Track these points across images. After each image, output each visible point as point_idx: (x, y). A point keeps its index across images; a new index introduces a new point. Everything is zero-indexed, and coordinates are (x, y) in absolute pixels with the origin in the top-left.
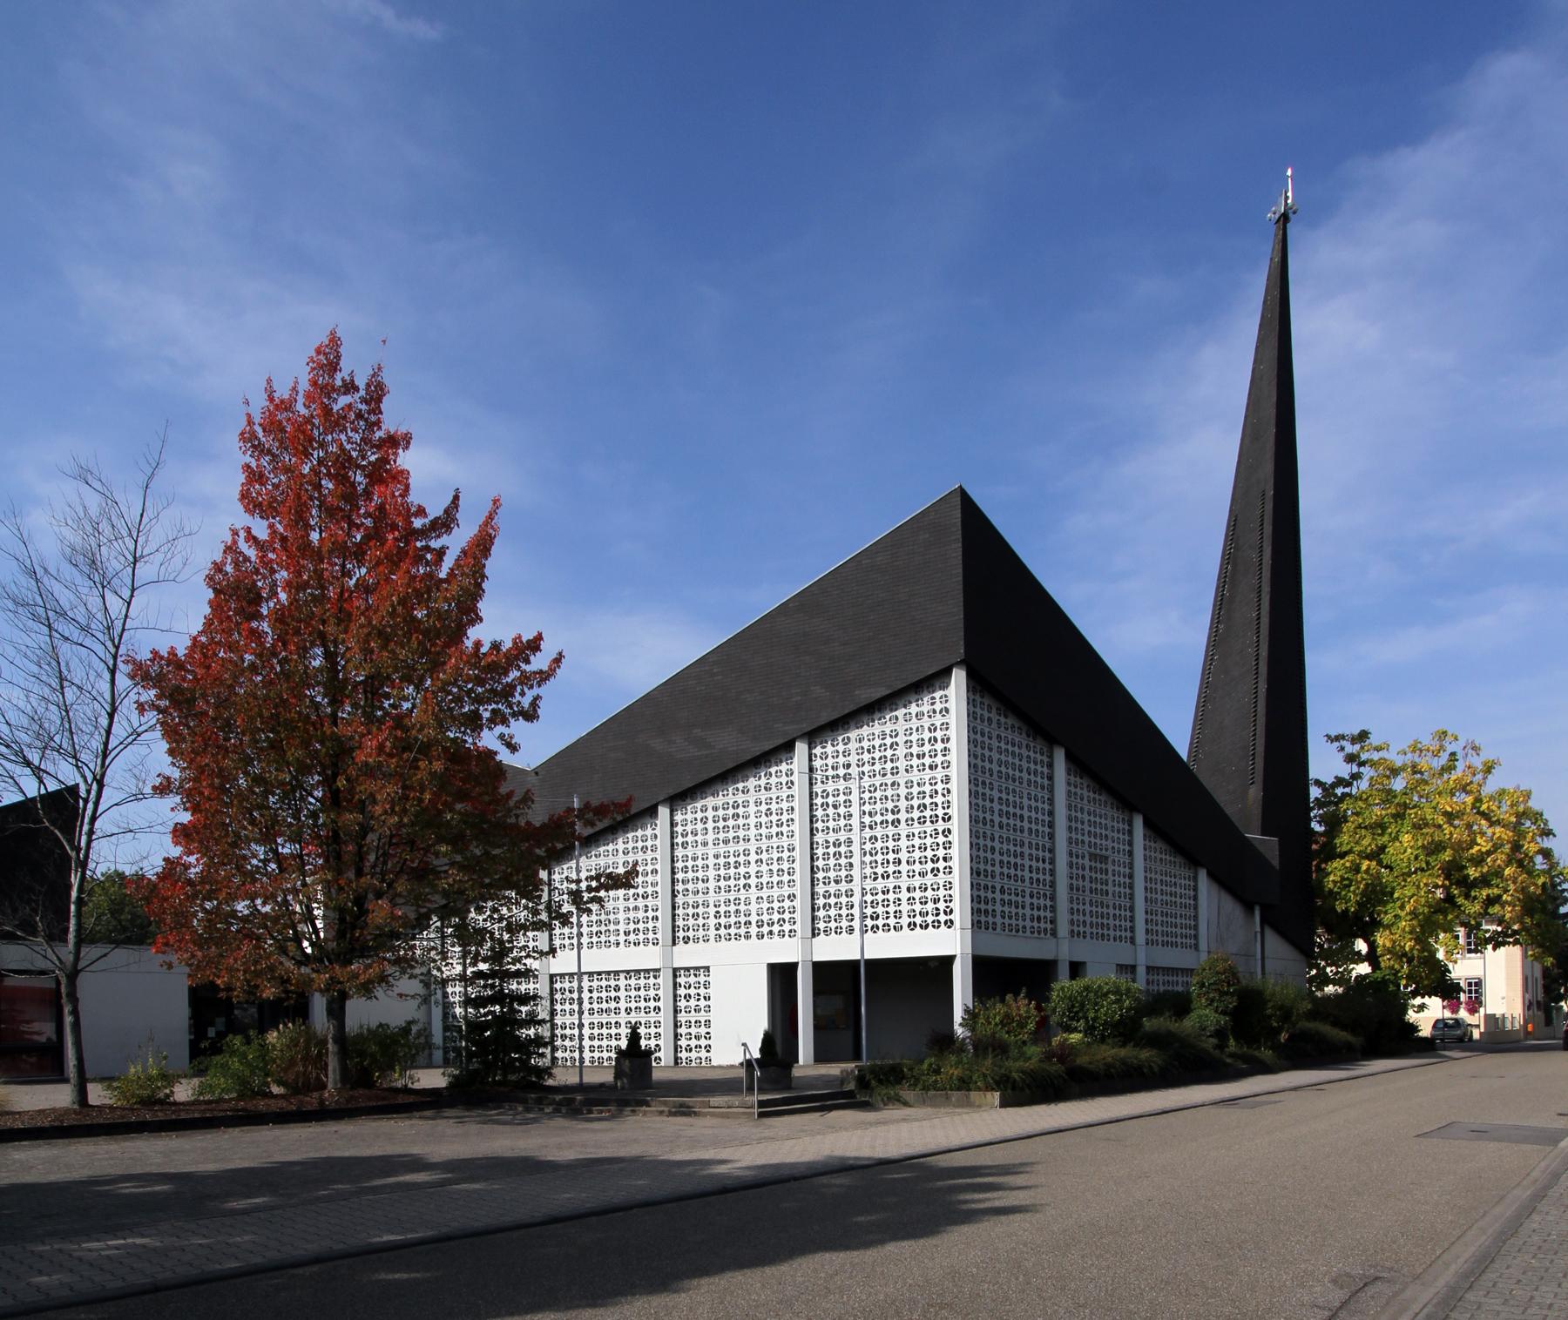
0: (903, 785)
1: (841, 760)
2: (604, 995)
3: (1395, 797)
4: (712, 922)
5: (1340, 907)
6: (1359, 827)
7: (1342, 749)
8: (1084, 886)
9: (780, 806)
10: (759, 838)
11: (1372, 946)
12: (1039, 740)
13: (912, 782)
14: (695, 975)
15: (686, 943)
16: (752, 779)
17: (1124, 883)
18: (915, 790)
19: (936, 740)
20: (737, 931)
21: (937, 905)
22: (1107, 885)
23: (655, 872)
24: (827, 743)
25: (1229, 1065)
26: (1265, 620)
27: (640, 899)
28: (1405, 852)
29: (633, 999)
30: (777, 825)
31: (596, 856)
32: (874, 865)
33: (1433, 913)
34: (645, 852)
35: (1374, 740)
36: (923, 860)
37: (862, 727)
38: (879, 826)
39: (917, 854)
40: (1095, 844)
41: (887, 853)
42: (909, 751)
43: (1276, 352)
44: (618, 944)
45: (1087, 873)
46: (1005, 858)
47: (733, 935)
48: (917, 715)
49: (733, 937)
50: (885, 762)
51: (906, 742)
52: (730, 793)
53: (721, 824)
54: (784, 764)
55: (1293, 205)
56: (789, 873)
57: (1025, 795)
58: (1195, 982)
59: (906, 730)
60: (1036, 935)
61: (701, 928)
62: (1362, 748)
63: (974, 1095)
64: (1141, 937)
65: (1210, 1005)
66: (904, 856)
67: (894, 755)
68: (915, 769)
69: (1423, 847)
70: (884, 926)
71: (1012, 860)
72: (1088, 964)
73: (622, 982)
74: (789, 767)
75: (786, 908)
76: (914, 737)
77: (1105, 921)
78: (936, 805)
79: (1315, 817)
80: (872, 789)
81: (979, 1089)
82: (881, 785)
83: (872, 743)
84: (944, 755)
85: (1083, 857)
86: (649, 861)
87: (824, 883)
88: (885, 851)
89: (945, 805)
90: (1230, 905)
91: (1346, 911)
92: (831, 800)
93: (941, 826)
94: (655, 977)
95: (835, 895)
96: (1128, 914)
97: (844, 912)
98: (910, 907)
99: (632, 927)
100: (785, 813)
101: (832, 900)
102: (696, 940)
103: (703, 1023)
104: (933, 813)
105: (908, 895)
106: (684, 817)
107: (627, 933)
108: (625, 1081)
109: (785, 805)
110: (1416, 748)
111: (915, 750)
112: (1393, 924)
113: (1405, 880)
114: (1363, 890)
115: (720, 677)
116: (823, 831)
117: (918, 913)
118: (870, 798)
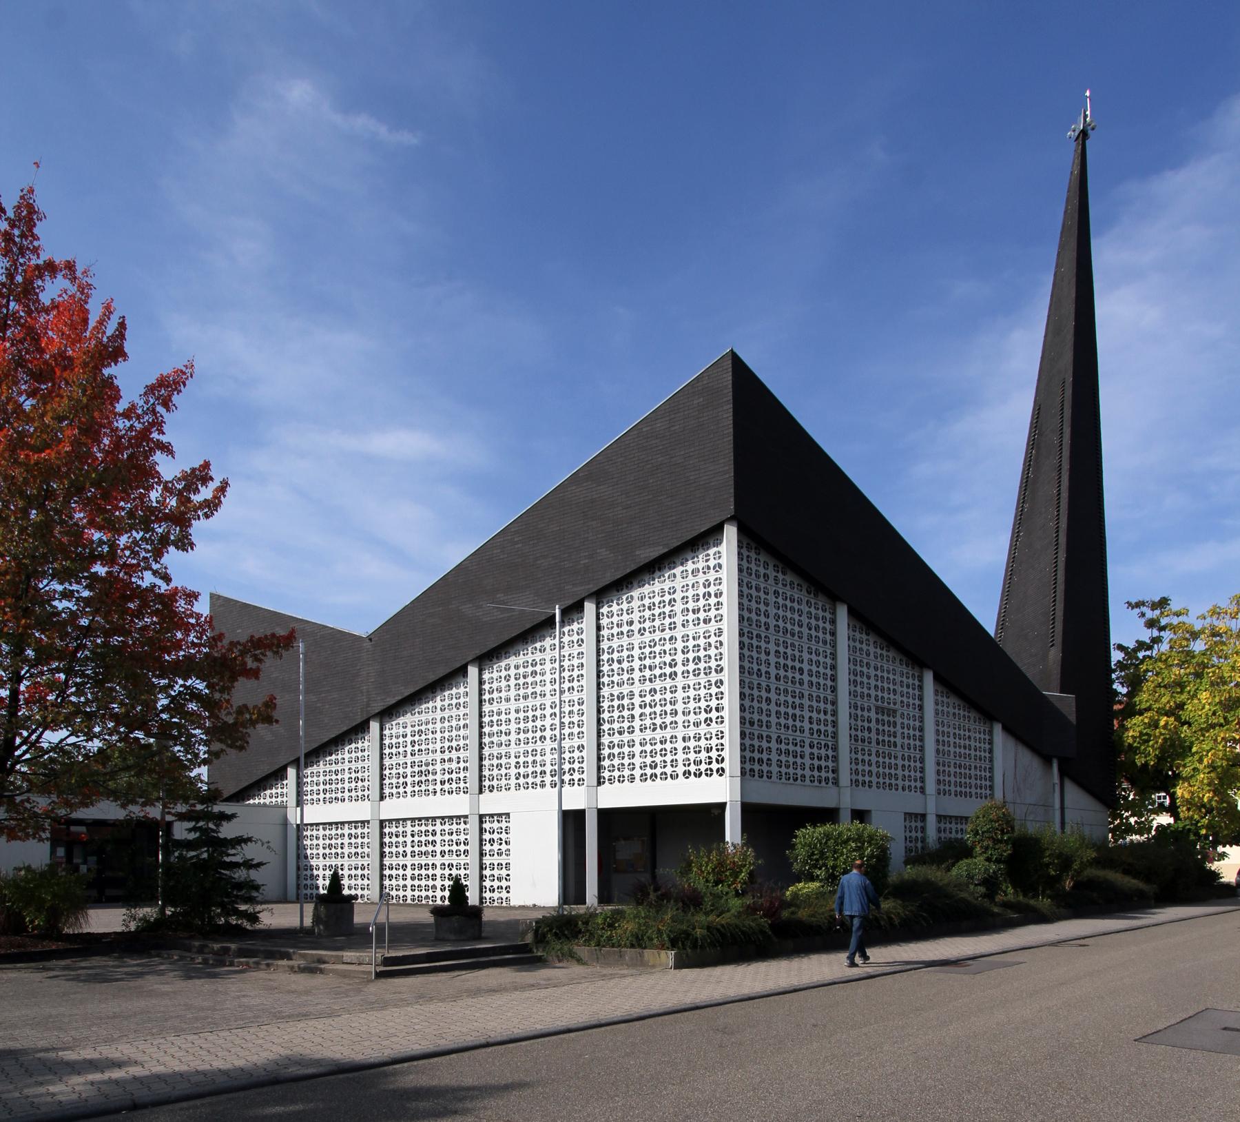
0: (679, 639)
1: (625, 617)
2: (423, 839)
3: (1193, 657)
4: (513, 771)
5: (1139, 761)
6: (1159, 686)
7: (1143, 615)
8: (870, 738)
9: (572, 662)
10: (553, 693)
11: (1173, 797)
12: (821, 597)
13: (688, 636)
14: (498, 821)
15: (491, 791)
16: (548, 639)
17: (914, 735)
18: (691, 643)
19: (710, 595)
20: (534, 780)
21: (710, 754)
22: (895, 737)
23: (465, 726)
24: (612, 602)
25: (998, 914)
26: (1065, 495)
27: (454, 751)
28: (1203, 708)
29: (447, 843)
30: (569, 681)
31: (419, 712)
32: (653, 716)
33: (1232, 766)
34: (458, 709)
35: (1174, 606)
36: (697, 710)
37: (644, 585)
38: (658, 679)
39: (692, 705)
40: (882, 697)
41: (665, 705)
42: (685, 606)
43: (1075, 254)
44: (435, 792)
45: (873, 725)
46: (782, 709)
47: (530, 783)
48: (693, 572)
49: (530, 785)
50: (664, 618)
51: (683, 598)
52: (530, 652)
53: (521, 681)
54: (576, 623)
55: (1091, 121)
56: (579, 726)
57: (805, 650)
58: (969, 830)
59: (683, 587)
60: (816, 783)
61: (504, 778)
62: (1162, 613)
63: (648, 953)
64: (931, 787)
65: (985, 852)
66: (680, 707)
67: (672, 611)
68: (691, 623)
69: (1220, 702)
70: (661, 774)
71: (790, 711)
72: (873, 812)
73: (438, 828)
74: (580, 626)
75: (576, 758)
76: (690, 593)
77: (893, 772)
78: (710, 657)
79: (1117, 678)
80: (652, 644)
81: (653, 947)
82: (660, 640)
83: (652, 600)
84: (717, 609)
85: (869, 710)
86: (461, 717)
87: (609, 734)
88: (663, 702)
89: (718, 657)
90: (1027, 758)
91: (1146, 765)
92: (615, 656)
93: (714, 677)
94: (465, 823)
95: (618, 745)
96: (918, 764)
97: (626, 761)
98: (685, 756)
99: (447, 776)
100: (576, 669)
101: (616, 751)
102: (499, 789)
103: (504, 866)
104: (707, 665)
105: (684, 744)
106: (491, 675)
107: (442, 783)
108: (321, 927)
109: (576, 662)
110: (1216, 612)
111: (691, 605)
112: (1192, 776)
113: (1204, 736)
114: (1162, 745)
115: (520, 545)
116: (608, 685)
117: (692, 761)
118: (651, 653)
